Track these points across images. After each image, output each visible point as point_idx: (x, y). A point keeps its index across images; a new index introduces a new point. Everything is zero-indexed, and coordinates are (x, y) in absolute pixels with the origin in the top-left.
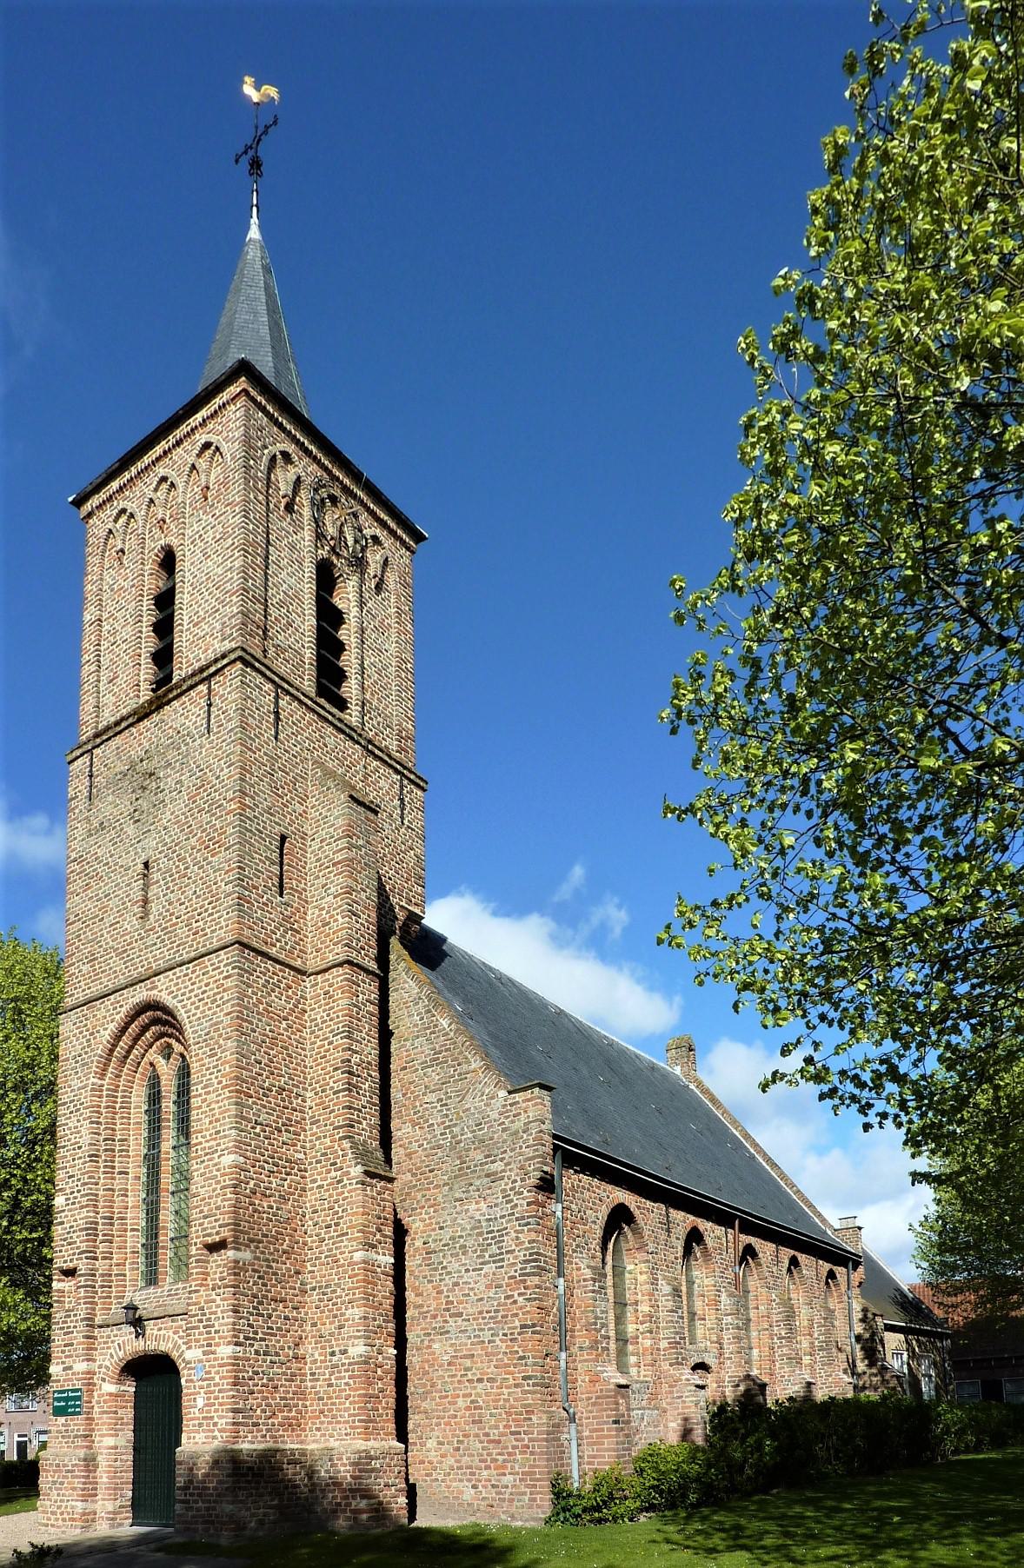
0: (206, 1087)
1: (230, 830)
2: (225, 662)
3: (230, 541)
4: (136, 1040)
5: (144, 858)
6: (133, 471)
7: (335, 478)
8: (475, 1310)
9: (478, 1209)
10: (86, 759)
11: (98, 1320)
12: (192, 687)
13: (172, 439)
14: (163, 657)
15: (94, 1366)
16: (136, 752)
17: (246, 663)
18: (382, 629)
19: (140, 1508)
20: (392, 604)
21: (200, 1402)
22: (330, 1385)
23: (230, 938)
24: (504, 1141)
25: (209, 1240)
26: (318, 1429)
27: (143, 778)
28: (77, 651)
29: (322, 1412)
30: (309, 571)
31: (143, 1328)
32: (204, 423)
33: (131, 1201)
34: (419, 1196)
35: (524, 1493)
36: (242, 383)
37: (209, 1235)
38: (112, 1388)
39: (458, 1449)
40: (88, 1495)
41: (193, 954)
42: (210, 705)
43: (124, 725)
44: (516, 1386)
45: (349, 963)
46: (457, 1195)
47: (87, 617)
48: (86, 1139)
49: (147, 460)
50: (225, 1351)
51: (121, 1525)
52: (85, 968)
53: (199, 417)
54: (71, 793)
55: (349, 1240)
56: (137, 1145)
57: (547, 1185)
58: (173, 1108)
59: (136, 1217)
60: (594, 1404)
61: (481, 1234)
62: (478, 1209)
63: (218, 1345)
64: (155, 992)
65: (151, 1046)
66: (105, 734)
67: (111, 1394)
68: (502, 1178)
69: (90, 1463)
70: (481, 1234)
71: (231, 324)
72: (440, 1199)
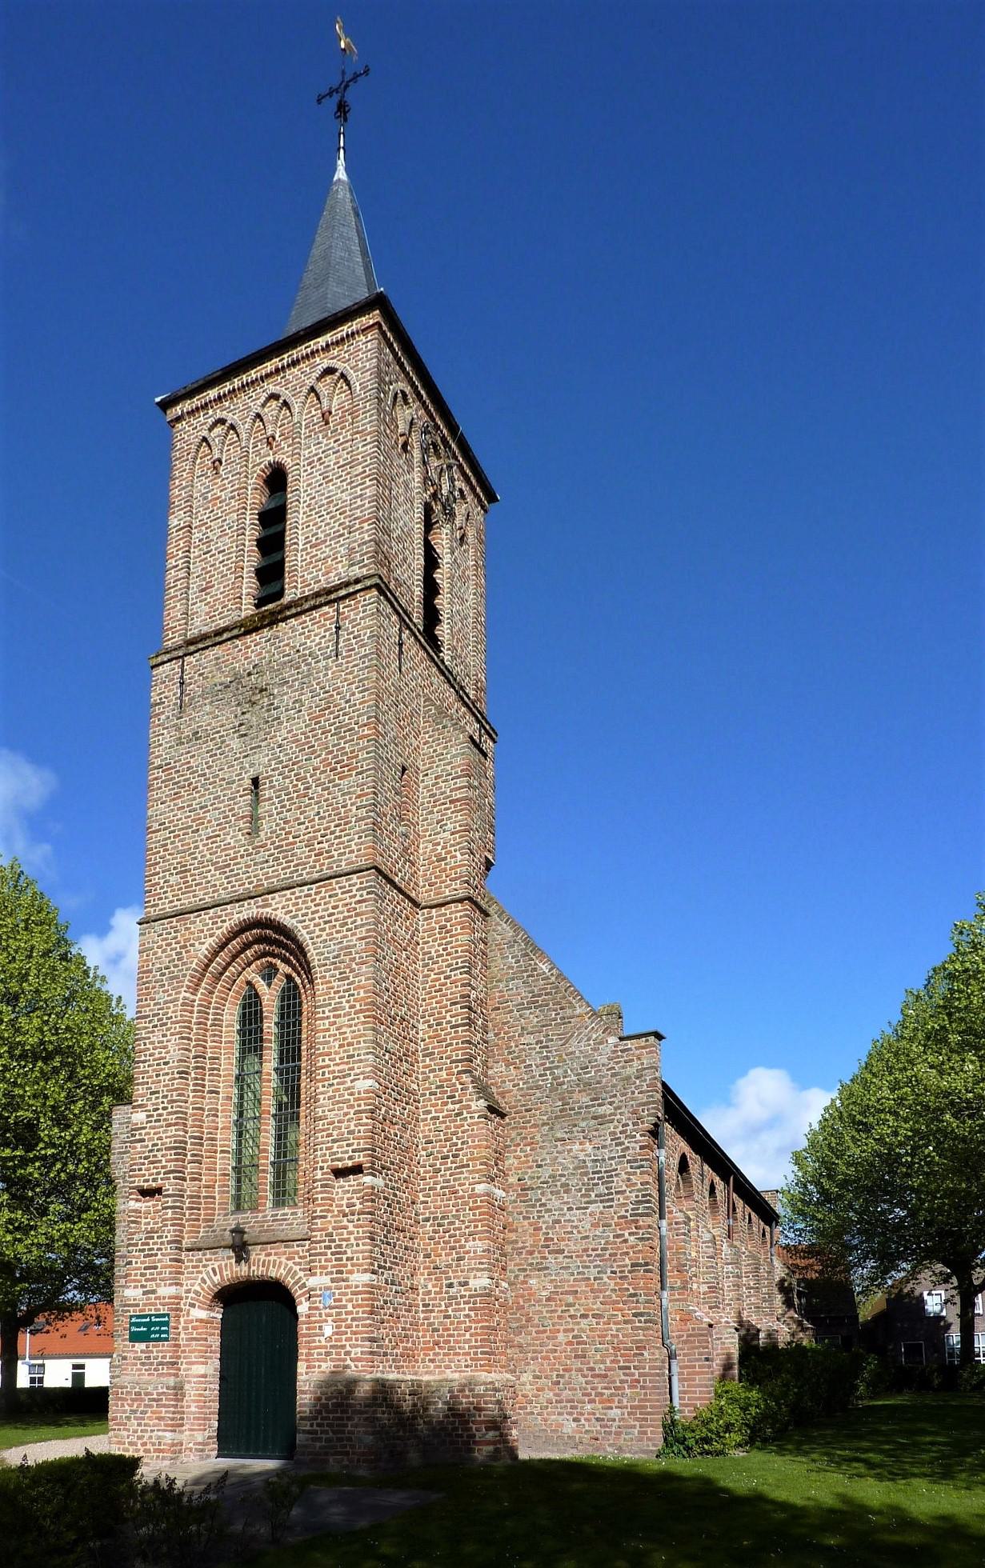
0: (335, 1009)
1: (363, 755)
2: (358, 587)
3: (360, 469)
4: (234, 957)
5: (252, 773)
6: (237, 382)
7: (437, 427)
8: (579, 1247)
9: (583, 1150)
10: (175, 665)
11: (186, 1242)
12: (315, 608)
13: (286, 358)
14: (271, 574)
15: (182, 1291)
16: (241, 665)
17: (381, 592)
18: (464, 579)
19: (229, 1440)
20: (471, 556)
21: (328, 1330)
22: (448, 1317)
23: (363, 862)
24: (614, 1086)
25: (340, 1165)
26: (432, 1361)
27: (252, 693)
28: (163, 556)
29: (437, 1343)
30: (418, 513)
31: (248, 1253)
32: (327, 348)
33: (221, 1122)
34: (513, 1135)
35: (634, 1427)
36: (374, 317)
37: (339, 1160)
38: (203, 1314)
39: (558, 1383)
40: (167, 1426)
41: (316, 876)
42: (338, 628)
43: (225, 636)
44: (626, 1322)
45: (470, 899)
46: (559, 1135)
47: (174, 521)
48: (174, 1053)
49: (253, 374)
50: (361, 1279)
51: (208, 1456)
52: (173, 880)
53: (322, 341)
54: (155, 698)
55: (471, 1172)
56: (228, 1065)
57: (655, 1133)
58: (274, 1030)
59: (227, 1139)
60: (685, 1342)
61: (586, 1174)
62: (583, 1150)
63: (351, 1272)
64: (268, 910)
65: (249, 965)
66: (197, 643)
67: (201, 1321)
68: (612, 1121)
69: (178, 1391)
70: (586, 1174)
71: (326, 257)
72: (538, 1138)
